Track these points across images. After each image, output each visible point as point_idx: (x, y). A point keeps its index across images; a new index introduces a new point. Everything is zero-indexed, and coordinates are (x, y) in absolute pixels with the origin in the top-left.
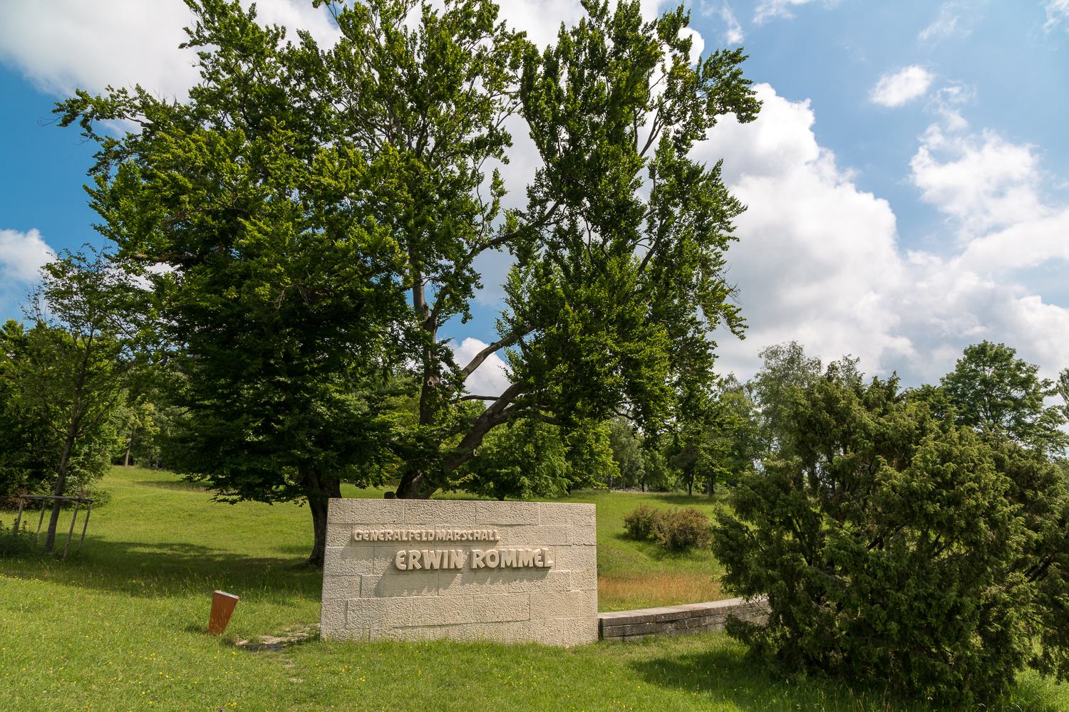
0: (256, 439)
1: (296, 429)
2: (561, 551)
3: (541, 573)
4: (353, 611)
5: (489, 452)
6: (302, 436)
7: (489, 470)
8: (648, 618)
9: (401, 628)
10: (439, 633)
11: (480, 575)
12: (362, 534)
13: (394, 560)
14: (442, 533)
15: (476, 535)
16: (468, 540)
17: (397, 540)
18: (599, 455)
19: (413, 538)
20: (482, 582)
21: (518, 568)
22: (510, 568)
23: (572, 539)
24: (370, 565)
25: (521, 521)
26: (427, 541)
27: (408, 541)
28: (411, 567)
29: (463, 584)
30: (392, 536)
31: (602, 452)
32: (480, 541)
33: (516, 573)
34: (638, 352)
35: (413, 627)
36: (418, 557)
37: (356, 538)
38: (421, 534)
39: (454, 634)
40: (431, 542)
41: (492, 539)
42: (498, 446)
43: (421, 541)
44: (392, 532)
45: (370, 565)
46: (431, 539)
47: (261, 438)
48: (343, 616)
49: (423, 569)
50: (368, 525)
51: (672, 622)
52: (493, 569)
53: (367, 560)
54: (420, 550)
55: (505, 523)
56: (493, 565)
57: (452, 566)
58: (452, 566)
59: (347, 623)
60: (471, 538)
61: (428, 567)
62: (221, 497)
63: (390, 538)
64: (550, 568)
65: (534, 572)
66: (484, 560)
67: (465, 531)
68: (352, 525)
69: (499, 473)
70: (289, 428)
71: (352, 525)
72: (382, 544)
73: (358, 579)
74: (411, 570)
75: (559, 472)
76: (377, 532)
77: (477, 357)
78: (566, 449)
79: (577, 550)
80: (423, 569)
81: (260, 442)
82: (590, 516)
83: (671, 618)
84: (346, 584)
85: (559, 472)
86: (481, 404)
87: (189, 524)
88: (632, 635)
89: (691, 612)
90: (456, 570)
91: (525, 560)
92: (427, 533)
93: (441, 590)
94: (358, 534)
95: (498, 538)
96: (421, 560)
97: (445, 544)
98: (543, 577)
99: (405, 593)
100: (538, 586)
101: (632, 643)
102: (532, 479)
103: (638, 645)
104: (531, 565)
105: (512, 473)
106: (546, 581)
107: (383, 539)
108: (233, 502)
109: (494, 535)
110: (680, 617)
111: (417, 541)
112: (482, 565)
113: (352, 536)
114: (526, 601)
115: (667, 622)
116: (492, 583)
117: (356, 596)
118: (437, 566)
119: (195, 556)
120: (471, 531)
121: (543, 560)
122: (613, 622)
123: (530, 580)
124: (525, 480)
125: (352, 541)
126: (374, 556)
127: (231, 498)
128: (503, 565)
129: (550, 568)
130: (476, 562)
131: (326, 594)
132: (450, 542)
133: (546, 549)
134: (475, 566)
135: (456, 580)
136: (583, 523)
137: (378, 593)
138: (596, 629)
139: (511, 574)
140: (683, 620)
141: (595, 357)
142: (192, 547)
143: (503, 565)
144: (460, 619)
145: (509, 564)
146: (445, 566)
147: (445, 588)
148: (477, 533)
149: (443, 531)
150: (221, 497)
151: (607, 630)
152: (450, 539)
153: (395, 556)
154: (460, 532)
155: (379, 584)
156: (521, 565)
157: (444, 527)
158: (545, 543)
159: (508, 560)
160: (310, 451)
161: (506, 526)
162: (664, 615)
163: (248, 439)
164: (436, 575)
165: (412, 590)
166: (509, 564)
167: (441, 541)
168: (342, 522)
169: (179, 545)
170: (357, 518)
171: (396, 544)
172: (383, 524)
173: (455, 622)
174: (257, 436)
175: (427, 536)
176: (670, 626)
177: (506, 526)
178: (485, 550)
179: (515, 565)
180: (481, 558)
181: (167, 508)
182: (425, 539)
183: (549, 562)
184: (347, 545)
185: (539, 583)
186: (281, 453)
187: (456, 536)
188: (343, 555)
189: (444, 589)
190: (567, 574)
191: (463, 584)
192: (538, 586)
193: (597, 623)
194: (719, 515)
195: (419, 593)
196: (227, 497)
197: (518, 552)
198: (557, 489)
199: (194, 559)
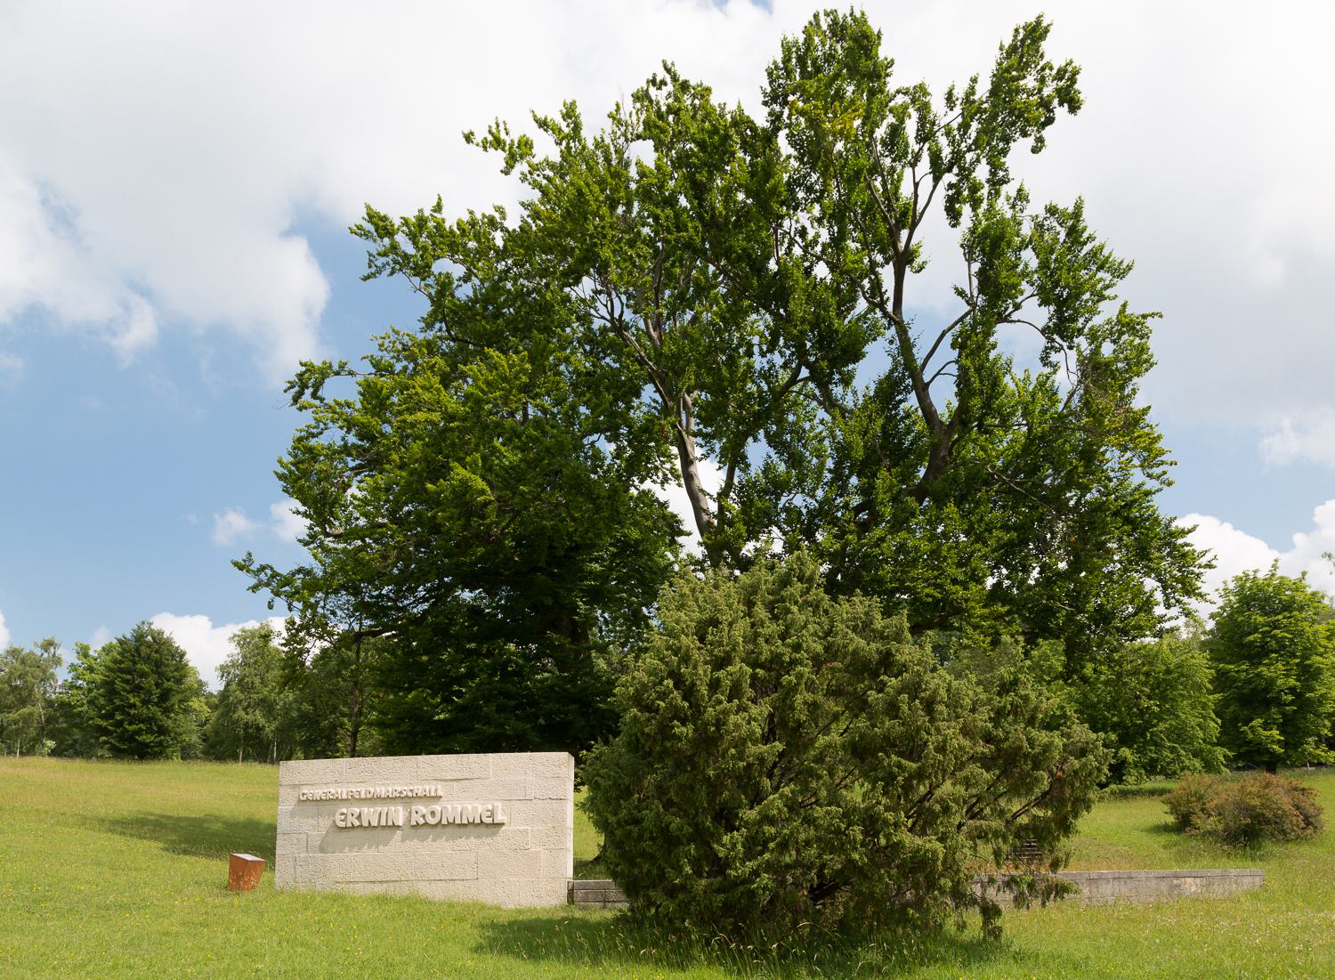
3: (493, 829)
14: (382, 791)
15: (416, 791)
20: (423, 839)
23: (531, 794)
26: (366, 799)
27: (347, 800)
29: (403, 841)
36: (356, 815)
41: (433, 794)
44: (333, 791)
52: (433, 826)
53: (312, 818)
60: (410, 794)
65: (483, 829)
76: (318, 792)
90: (395, 827)
93: (381, 847)
94: (303, 794)
96: (359, 817)
98: (494, 834)
99: (347, 850)
104: (477, 821)
121: (492, 816)
123: (479, 837)
125: (299, 800)
126: (319, 815)
137: (322, 850)
139: (457, 830)
149: (383, 788)
154: (399, 789)
156: (465, 822)
159: (450, 816)
165: (353, 846)
171: (338, 802)
179: (458, 821)
182: (363, 796)
185: (489, 840)
188: (293, 814)
191: (403, 841)
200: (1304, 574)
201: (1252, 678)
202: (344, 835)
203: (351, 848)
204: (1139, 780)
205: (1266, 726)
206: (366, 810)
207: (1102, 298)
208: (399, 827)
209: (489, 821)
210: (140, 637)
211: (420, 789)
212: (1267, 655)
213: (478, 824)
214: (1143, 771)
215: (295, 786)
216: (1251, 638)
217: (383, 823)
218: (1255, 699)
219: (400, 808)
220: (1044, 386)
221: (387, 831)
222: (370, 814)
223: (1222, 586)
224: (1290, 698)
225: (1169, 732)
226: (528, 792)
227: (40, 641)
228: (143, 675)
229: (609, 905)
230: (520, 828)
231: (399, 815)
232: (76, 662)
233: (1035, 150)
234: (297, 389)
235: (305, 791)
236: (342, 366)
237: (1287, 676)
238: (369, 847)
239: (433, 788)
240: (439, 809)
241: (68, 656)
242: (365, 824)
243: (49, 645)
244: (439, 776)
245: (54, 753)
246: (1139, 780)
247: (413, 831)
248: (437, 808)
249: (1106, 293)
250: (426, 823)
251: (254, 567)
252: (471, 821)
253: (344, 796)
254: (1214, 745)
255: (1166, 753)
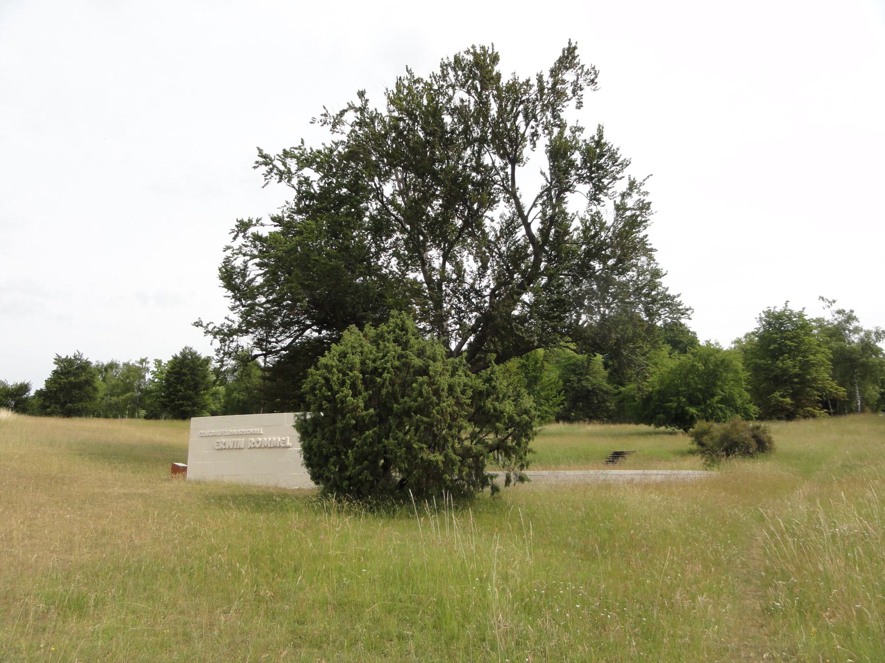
14: (235, 431)
96: (225, 444)
200: (804, 309)
205: (783, 396)
207: (615, 179)
209: (283, 445)
210: (184, 354)
212: (782, 355)
218: (780, 380)
220: (596, 220)
222: (229, 441)
223: (758, 316)
225: (721, 401)
227: (139, 360)
228: (185, 375)
231: (242, 441)
232: (156, 370)
233: (578, 108)
234: (236, 233)
236: (258, 221)
241: (152, 367)
243: (143, 361)
245: (146, 417)
249: (618, 176)
251: (205, 325)
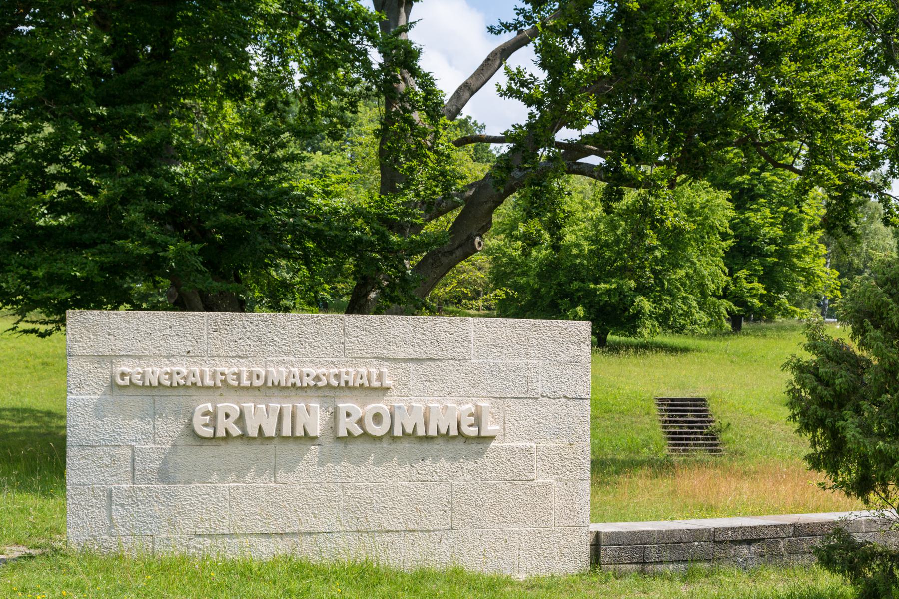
0: (55, 223)
1: (124, 201)
2: (518, 408)
3: (475, 447)
4: (122, 505)
5: (575, 251)
6: (134, 215)
7: (576, 285)
8: (695, 534)
9: (210, 536)
10: (279, 548)
11: (356, 448)
12: (130, 374)
13: (191, 420)
14: (279, 373)
15: (344, 377)
16: (329, 386)
17: (194, 384)
18: (798, 257)
19: (224, 382)
20: (359, 461)
21: (427, 438)
22: (411, 437)
23: (540, 387)
24: (149, 428)
25: (434, 353)
26: (251, 388)
27: (215, 387)
28: (221, 433)
29: (321, 463)
30: (185, 378)
31: (804, 250)
32: (353, 388)
33: (426, 446)
34: (776, 26)
35: (231, 535)
36: (235, 416)
37: (119, 381)
38: (238, 376)
39: (307, 551)
40: (258, 388)
41: (375, 384)
42: (594, 240)
43: (240, 388)
44: (185, 371)
45: (149, 428)
46: (257, 383)
47: (63, 219)
48: (104, 514)
49: (244, 437)
50: (140, 358)
51: (749, 542)
52: (380, 438)
53: (142, 419)
54: (238, 403)
55: (402, 356)
56: (378, 431)
57: (300, 432)
58: (300, 432)
59: (112, 526)
60: (334, 383)
61: (253, 432)
62: (23, 326)
63: (182, 382)
64: (492, 438)
65: (460, 446)
66: (360, 422)
67: (324, 370)
68: (111, 358)
69: (596, 290)
70: (109, 199)
71: (111, 358)
72: (168, 392)
73: (128, 453)
74: (222, 439)
75: (712, 286)
76: (156, 372)
77: (488, 60)
78: (724, 244)
79: (550, 407)
80: (279, 436)
81: (60, 226)
82: (579, 344)
83: (748, 536)
84: (107, 460)
85: (712, 286)
86: (485, 149)
87: (41, 379)
88: (661, 562)
89: (794, 525)
90: (308, 438)
91: (442, 422)
92: (251, 373)
93: (280, 474)
94: (123, 375)
95: (387, 382)
96: (241, 420)
97: (286, 393)
98: (479, 454)
99: (215, 477)
100: (469, 471)
101: (655, 575)
102: (657, 301)
103: (671, 579)
104: (454, 432)
105: (619, 290)
106: (486, 462)
107: (168, 383)
108: (48, 334)
109: (380, 377)
110: (771, 533)
111: (233, 387)
112: (357, 431)
113: (113, 378)
114: (445, 497)
115: (741, 542)
116: (377, 463)
117: (125, 480)
118: (270, 431)
119: (30, 427)
120: (335, 371)
121: (478, 423)
122: (617, 539)
123: (454, 459)
124: (645, 304)
125: (113, 385)
126: (155, 413)
127: (43, 328)
128: (397, 432)
129: (492, 438)
130: (345, 426)
131: (72, 476)
132: (296, 389)
133: (485, 404)
134: (343, 433)
135: (308, 457)
136: (563, 358)
137: (164, 476)
138: (586, 549)
139: (416, 447)
140: (775, 540)
141: (683, 41)
142: (31, 412)
143: (397, 432)
144: (311, 524)
145: (409, 430)
146: (286, 431)
147: (288, 471)
148: (347, 373)
149: (282, 369)
150: (23, 326)
151: (607, 553)
152: (294, 385)
153: (193, 414)
154: (314, 372)
155: (165, 462)
156: (432, 432)
157: (283, 362)
158: (484, 393)
159: (408, 422)
160: (152, 243)
161: (406, 361)
162: (734, 529)
163: (41, 222)
164: (270, 447)
165: (228, 471)
166: (409, 430)
167: (278, 387)
168: (91, 352)
169: (13, 409)
170: (120, 346)
171: (193, 392)
172: (168, 357)
173: (308, 529)
174: (56, 218)
175: (250, 378)
176: (744, 550)
177: (406, 361)
178: (363, 405)
179: (421, 432)
180: (355, 418)
181: (9, 352)
182: (245, 383)
183: (490, 428)
184: (104, 394)
185: (471, 465)
186: (105, 247)
187: (305, 379)
188: (99, 411)
189: (287, 472)
190: (529, 450)
191: (321, 463)
192: (469, 471)
193: (588, 540)
194: (812, 337)
195: (240, 477)
196: (37, 326)
197: (428, 409)
198: (706, 319)
199: (28, 432)
201: (738, 223)
202: (208, 451)
203: (224, 474)
204: (653, 333)
206: (249, 406)
208: (314, 438)
209: (472, 432)
211: (352, 373)
213: (454, 437)
214: (656, 324)
215: (101, 358)
216: (739, 179)
217: (286, 431)
219: (315, 405)
221: (291, 446)
224: (773, 248)
226: (533, 385)
229: (649, 567)
230: (522, 444)
235: (127, 370)
237: (772, 224)
238: (259, 474)
239: (374, 372)
240: (387, 409)
242: (253, 432)
244: (384, 352)
246: (653, 333)
247: (340, 446)
248: (381, 406)
250: (365, 434)
252: (443, 431)
253: (208, 382)
254: (719, 298)
255: (679, 303)
